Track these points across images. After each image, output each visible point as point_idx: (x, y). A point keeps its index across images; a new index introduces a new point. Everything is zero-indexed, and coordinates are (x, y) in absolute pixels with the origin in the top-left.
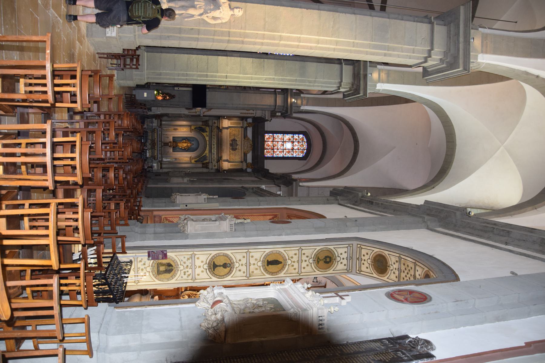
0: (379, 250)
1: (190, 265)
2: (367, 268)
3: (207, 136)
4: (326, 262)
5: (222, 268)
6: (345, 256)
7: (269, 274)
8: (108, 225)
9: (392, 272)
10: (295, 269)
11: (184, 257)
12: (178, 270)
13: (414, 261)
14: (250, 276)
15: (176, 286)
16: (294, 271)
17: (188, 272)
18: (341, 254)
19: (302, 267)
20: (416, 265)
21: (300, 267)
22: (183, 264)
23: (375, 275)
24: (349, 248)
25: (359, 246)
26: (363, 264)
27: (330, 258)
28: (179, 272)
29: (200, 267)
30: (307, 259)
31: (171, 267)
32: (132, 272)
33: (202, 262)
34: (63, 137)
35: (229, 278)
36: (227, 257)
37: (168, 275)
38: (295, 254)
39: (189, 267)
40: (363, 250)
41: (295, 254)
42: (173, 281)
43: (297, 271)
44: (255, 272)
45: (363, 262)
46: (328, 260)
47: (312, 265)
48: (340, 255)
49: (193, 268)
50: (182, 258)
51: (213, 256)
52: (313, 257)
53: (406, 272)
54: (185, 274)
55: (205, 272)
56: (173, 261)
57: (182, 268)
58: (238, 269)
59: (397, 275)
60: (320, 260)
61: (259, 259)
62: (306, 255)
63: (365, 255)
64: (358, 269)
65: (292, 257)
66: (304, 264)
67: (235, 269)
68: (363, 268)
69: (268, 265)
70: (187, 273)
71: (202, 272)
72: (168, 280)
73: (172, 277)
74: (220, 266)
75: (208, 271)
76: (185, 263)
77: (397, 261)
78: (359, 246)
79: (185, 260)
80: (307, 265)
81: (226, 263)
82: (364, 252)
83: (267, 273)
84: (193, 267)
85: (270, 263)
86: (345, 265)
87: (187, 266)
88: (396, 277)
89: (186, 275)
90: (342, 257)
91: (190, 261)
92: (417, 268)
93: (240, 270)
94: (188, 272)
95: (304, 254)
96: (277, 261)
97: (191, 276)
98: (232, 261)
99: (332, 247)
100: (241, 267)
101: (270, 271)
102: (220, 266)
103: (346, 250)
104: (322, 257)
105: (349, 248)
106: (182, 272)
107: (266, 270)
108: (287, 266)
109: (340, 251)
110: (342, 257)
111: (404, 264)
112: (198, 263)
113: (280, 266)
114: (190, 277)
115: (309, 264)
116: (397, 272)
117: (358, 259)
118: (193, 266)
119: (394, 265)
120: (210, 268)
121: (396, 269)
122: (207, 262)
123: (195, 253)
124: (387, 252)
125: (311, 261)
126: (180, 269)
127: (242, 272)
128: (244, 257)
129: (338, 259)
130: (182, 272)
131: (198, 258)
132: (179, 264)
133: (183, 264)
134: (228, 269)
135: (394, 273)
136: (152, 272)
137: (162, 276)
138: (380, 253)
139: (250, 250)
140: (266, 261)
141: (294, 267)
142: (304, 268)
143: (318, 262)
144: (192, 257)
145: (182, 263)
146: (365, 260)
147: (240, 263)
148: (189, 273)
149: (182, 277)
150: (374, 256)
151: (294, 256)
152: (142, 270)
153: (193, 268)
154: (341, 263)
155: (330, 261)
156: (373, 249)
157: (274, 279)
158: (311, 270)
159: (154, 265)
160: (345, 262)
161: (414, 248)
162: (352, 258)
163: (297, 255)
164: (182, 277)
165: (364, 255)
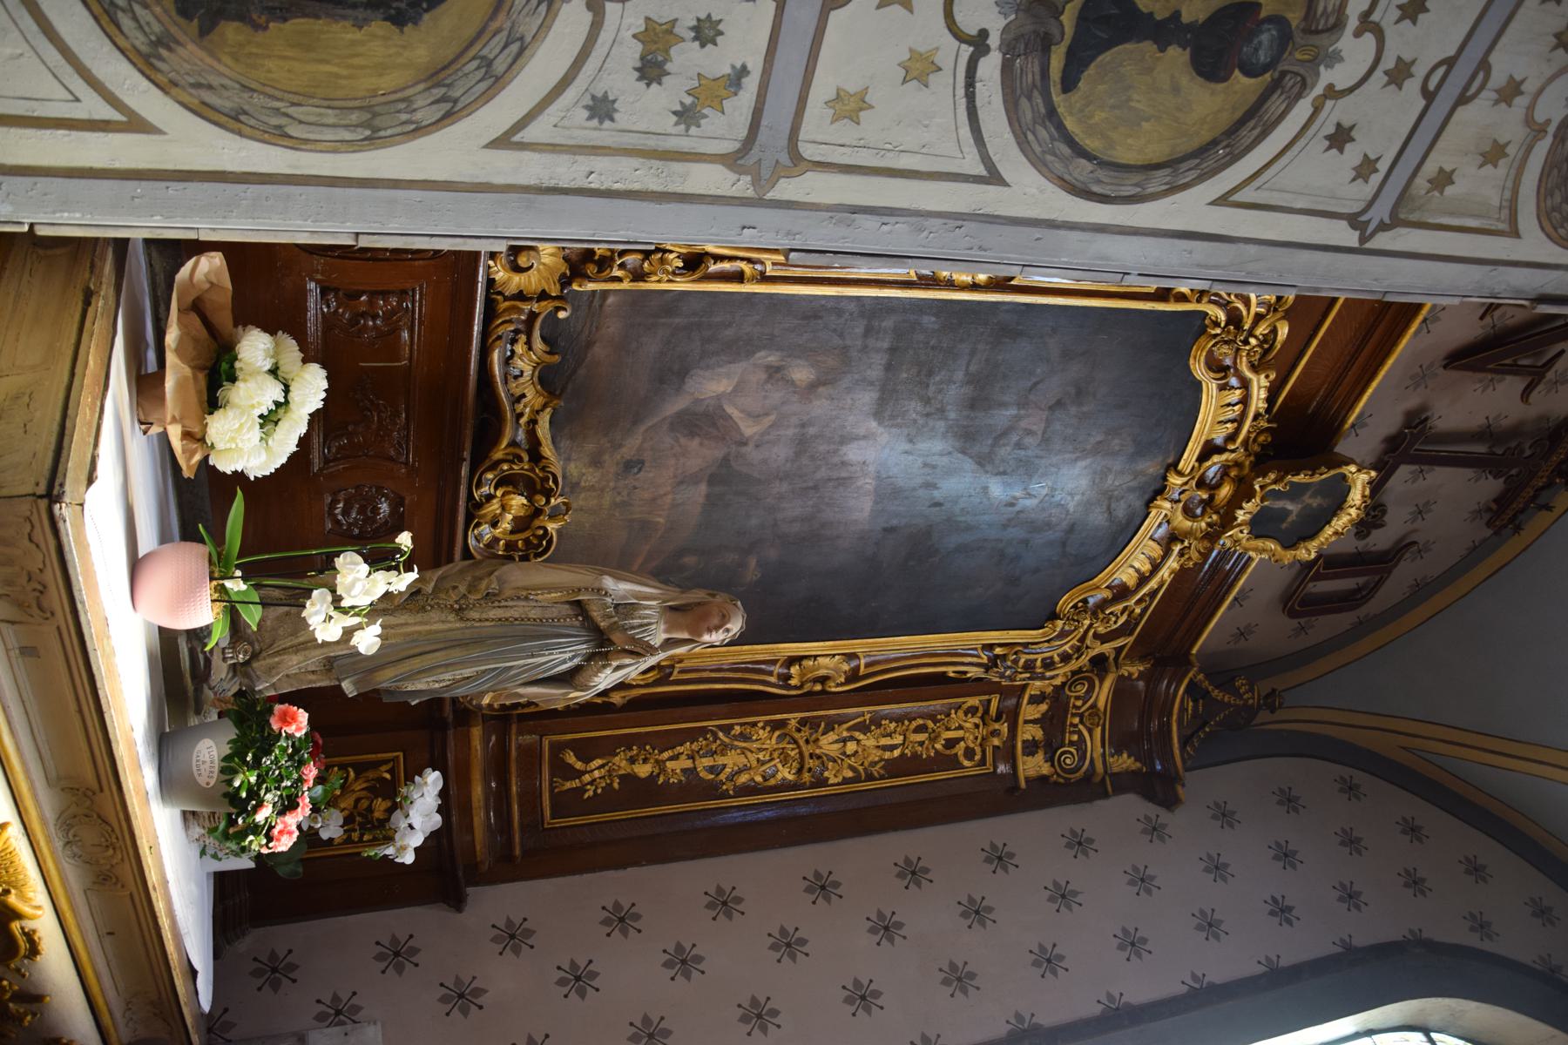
32: (216, 770)
34: (127, 240)
35: (1190, 207)
54: (651, 70)
55: (945, 91)
67: (1303, 109)
70: (687, 59)
72: (376, 123)
73: (447, 92)
75: (990, 67)
110: (1509, 125)
114: (725, 126)
148: (716, 61)
149: (602, 109)
159: (716, 621)
164: (602, 109)
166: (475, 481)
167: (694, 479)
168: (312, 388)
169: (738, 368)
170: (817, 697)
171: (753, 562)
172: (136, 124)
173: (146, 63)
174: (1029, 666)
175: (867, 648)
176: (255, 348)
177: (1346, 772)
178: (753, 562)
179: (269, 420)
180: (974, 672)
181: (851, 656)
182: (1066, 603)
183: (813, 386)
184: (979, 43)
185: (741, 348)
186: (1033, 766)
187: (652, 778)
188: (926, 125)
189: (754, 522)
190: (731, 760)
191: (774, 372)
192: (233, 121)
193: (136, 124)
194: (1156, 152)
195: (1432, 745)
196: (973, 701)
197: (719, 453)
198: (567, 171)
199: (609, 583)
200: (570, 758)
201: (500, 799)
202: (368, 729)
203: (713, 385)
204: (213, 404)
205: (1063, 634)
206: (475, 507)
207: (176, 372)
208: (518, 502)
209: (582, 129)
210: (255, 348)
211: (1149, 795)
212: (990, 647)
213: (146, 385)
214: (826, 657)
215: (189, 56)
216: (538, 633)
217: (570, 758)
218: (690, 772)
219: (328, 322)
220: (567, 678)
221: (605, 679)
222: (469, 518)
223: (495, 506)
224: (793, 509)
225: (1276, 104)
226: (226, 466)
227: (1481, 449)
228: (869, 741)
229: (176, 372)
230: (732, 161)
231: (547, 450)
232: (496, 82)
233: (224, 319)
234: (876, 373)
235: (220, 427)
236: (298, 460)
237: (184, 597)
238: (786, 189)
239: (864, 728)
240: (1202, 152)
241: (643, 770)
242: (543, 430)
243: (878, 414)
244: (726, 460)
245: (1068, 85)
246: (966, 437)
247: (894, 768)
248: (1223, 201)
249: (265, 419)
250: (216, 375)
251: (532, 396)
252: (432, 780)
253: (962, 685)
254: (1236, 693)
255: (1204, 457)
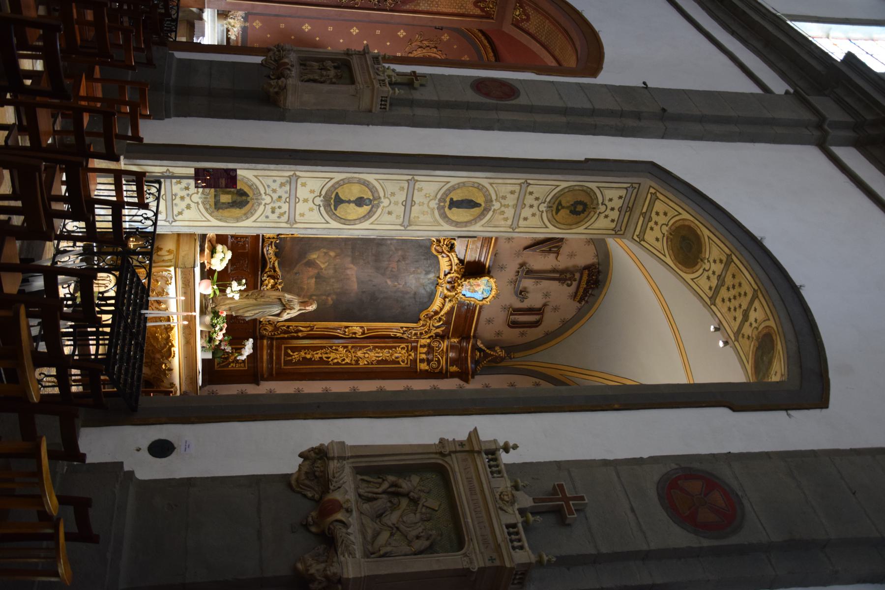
0: (692, 219)
1: (285, 196)
2: (657, 240)
3: (421, 513)
4: (574, 212)
5: (352, 205)
6: (617, 203)
7: (451, 225)
8: (134, 252)
9: (706, 274)
10: (506, 219)
11: (274, 181)
12: (259, 204)
13: (756, 288)
14: (410, 225)
15: (253, 232)
16: (503, 223)
17: (280, 207)
18: (611, 200)
19: (522, 216)
20: (755, 297)
21: (517, 216)
22: (271, 193)
23: (668, 260)
24: (630, 190)
25: (652, 190)
26: (652, 229)
27: (585, 206)
28: (262, 207)
29: (306, 201)
30: (536, 203)
31: (244, 198)
33: (312, 192)
35: (366, 225)
36: (367, 186)
37: (236, 212)
38: (512, 192)
39: (283, 199)
40: (657, 203)
41: (512, 192)
42: (248, 223)
43: (509, 222)
44: (422, 218)
45: (651, 224)
46: (580, 208)
47: (544, 215)
48: (606, 202)
49: (292, 201)
50: (269, 181)
51: (337, 183)
52: (548, 200)
53: (733, 292)
54: (273, 212)
55: (316, 212)
56: (250, 187)
57: (268, 199)
58: (387, 210)
59: (714, 285)
60: (563, 208)
61: (433, 194)
62: (535, 195)
63: (661, 214)
64: (637, 233)
65: (504, 198)
66: (527, 212)
67: (379, 211)
68: (650, 236)
69: (450, 208)
70: (278, 211)
71: (311, 210)
72: (238, 220)
73: (247, 216)
74: (349, 202)
75: (322, 209)
76: (274, 191)
77: (721, 261)
78: (652, 190)
79: (275, 186)
80: (534, 215)
81: (361, 198)
82: (659, 206)
83: (447, 222)
84: (292, 198)
85: (454, 204)
86: (613, 221)
87: (280, 197)
88: (710, 288)
89: (276, 215)
90: (610, 205)
91: (287, 188)
92: (756, 304)
93: (390, 213)
94: (280, 207)
95: (531, 193)
96: (472, 201)
97: (286, 215)
98: (376, 195)
99: (593, 186)
100: (392, 208)
101: (454, 218)
102: (349, 202)
103: (623, 193)
104: (567, 201)
105: (630, 190)
106: (269, 207)
107: (444, 216)
108: (491, 213)
109: (608, 194)
110: (610, 205)
111: (734, 276)
112: (302, 193)
113: (476, 211)
115: (538, 213)
116: (714, 282)
117: (644, 215)
118: (293, 197)
119: (713, 264)
120: (327, 205)
121: (714, 273)
122: (323, 193)
123: (298, 173)
124: (706, 232)
125: (543, 207)
126: (263, 202)
127: (394, 215)
128: (402, 189)
129: (602, 208)
130: (269, 207)
131: (304, 185)
132: (262, 192)
133: (271, 193)
134: (366, 209)
135: (708, 278)
136: (203, 203)
137: (226, 213)
138: (692, 225)
139: (416, 178)
140: (448, 200)
141: (506, 216)
142: (525, 219)
143: (558, 211)
144: (292, 181)
145: (269, 191)
146: (656, 223)
147: (393, 199)
148: (282, 211)
150: (678, 224)
151: (509, 195)
152: (182, 198)
153: (292, 201)
154: (606, 216)
155: (584, 211)
156: (681, 210)
157: (459, 234)
158: (540, 224)
160: (615, 215)
161: (768, 244)
162: (631, 210)
163: (516, 195)
164: (267, 217)
165: (657, 214)
166: (262, 276)
167: (312, 277)
168: (229, 255)
169: (317, 253)
170: (353, 338)
171: (330, 299)
172: (209, 221)
173: (210, 214)
174: (416, 334)
175: (365, 325)
176: (219, 248)
177: (537, 380)
178: (330, 299)
179: (221, 260)
180: (398, 335)
181: (361, 327)
182: (422, 316)
183: (335, 256)
184: (319, 206)
185: (317, 248)
186: (424, 366)
187: (311, 359)
188: (315, 216)
189: (456, 340)
190: (332, 356)
191: (325, 253)
192: (220, 220)
193: (209, 221)
194: (355, 218)
195: (570, 374)
196: (403, 345)
197: (316, 271)
198: (263, 225)
199: (286, 295)
200: (289, 351)
201: (271, 355)
202: (239, 330)
203: (314, 256)
204: (212, 257)
205: (423, 326)
206: (262, 282)
207: (207, 251)
208: (272, 281)
209: (265, 219)
210: (219, 248)
211: (462, 379)
212: (402, 328)
213: (202, 251)
214: (356, 327)
215: (216, 213)
216: (271, 304)
217: (289, 351)
218: (321, 358)
219: (232, 243)
220: (278, 315)
221: (286, 316)
222: (261, 284)
223: (266, 282)
224: (337, 285)
225: (374, 209)
226: (213, 268)
227: (557, 275)
228: (372, 354)
229: (207, 251)
230: (286, 223)
231: (277, 269)
232: (253, 215)
233: (214, 243)
234: (350, 253)
235: (213, 261)
236: (226, 268)
237: (207, 287)
238: (295, 226)
239: (370, 350)
240: (364, 217)
241: (308, 356)
242: (276, 264)
243: (353, 263)
244: (318, 273)
245: (336, 209)
246: (377, 269)
247: (379, 362)
248: (372, 224)
249: (220, 260)
250: (213, 252)
251: (273, 258)
252: (251, 340)
253: (400, 340)
254: (496, 351)
255: (446, 275)
